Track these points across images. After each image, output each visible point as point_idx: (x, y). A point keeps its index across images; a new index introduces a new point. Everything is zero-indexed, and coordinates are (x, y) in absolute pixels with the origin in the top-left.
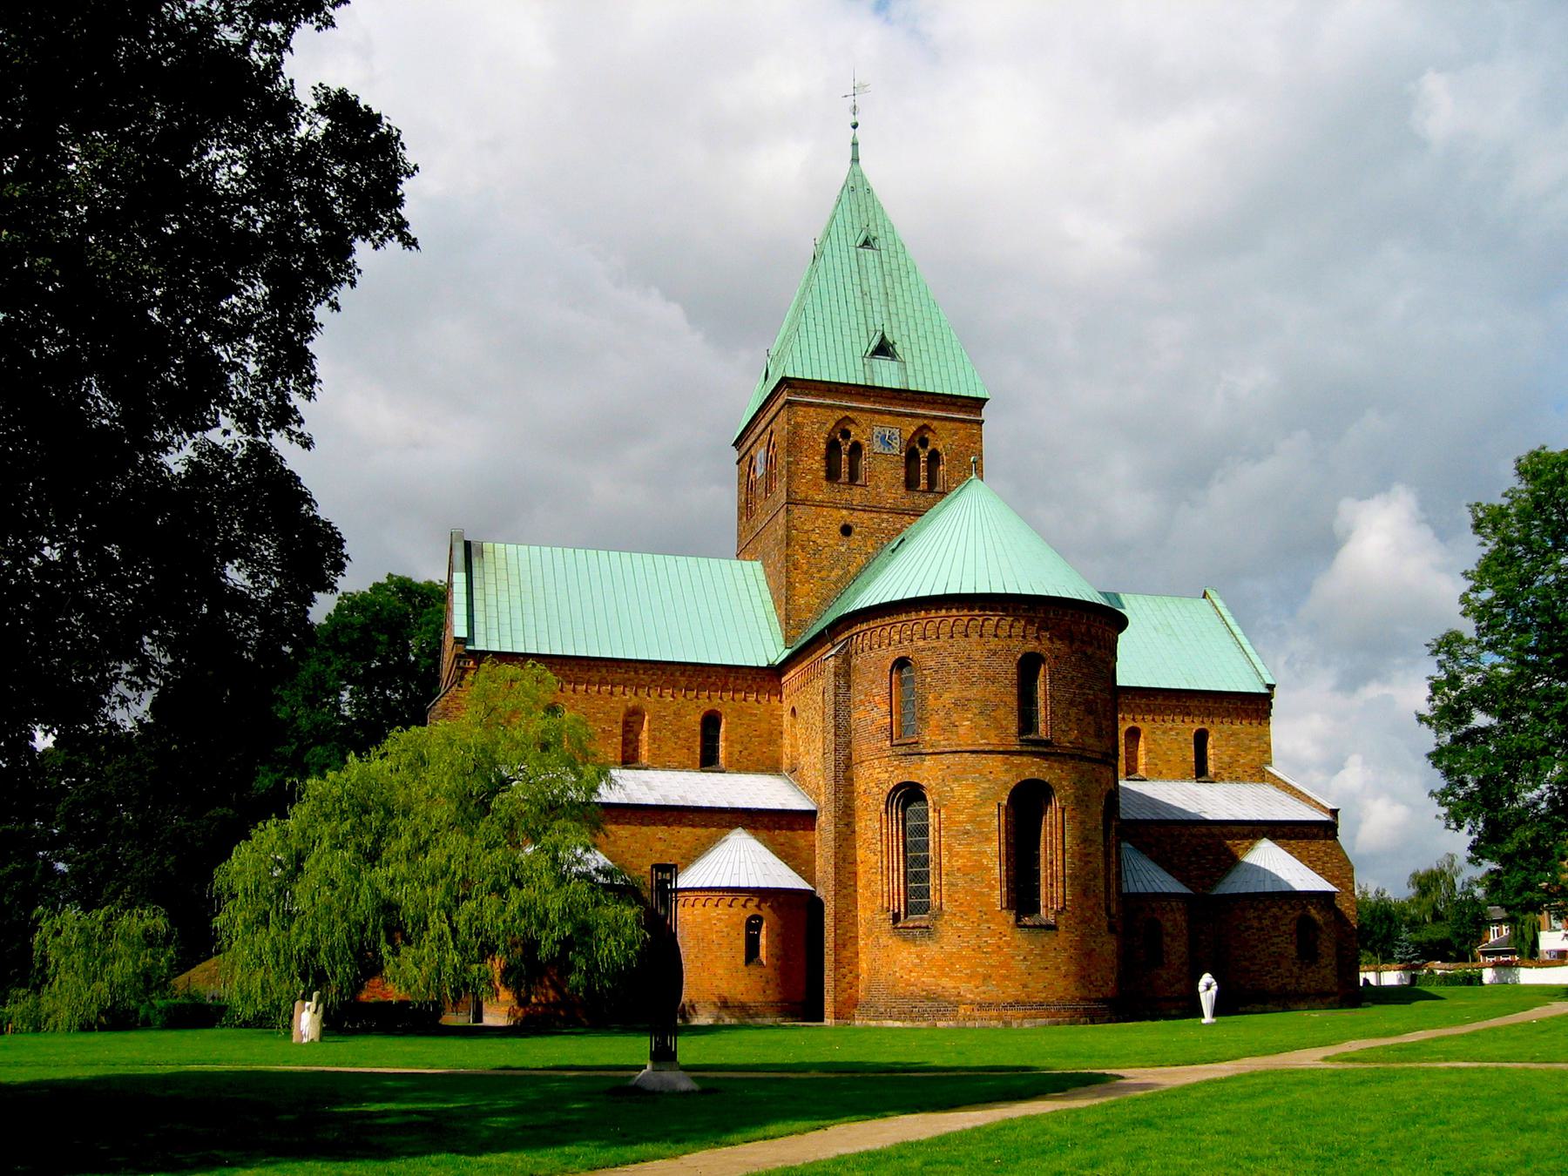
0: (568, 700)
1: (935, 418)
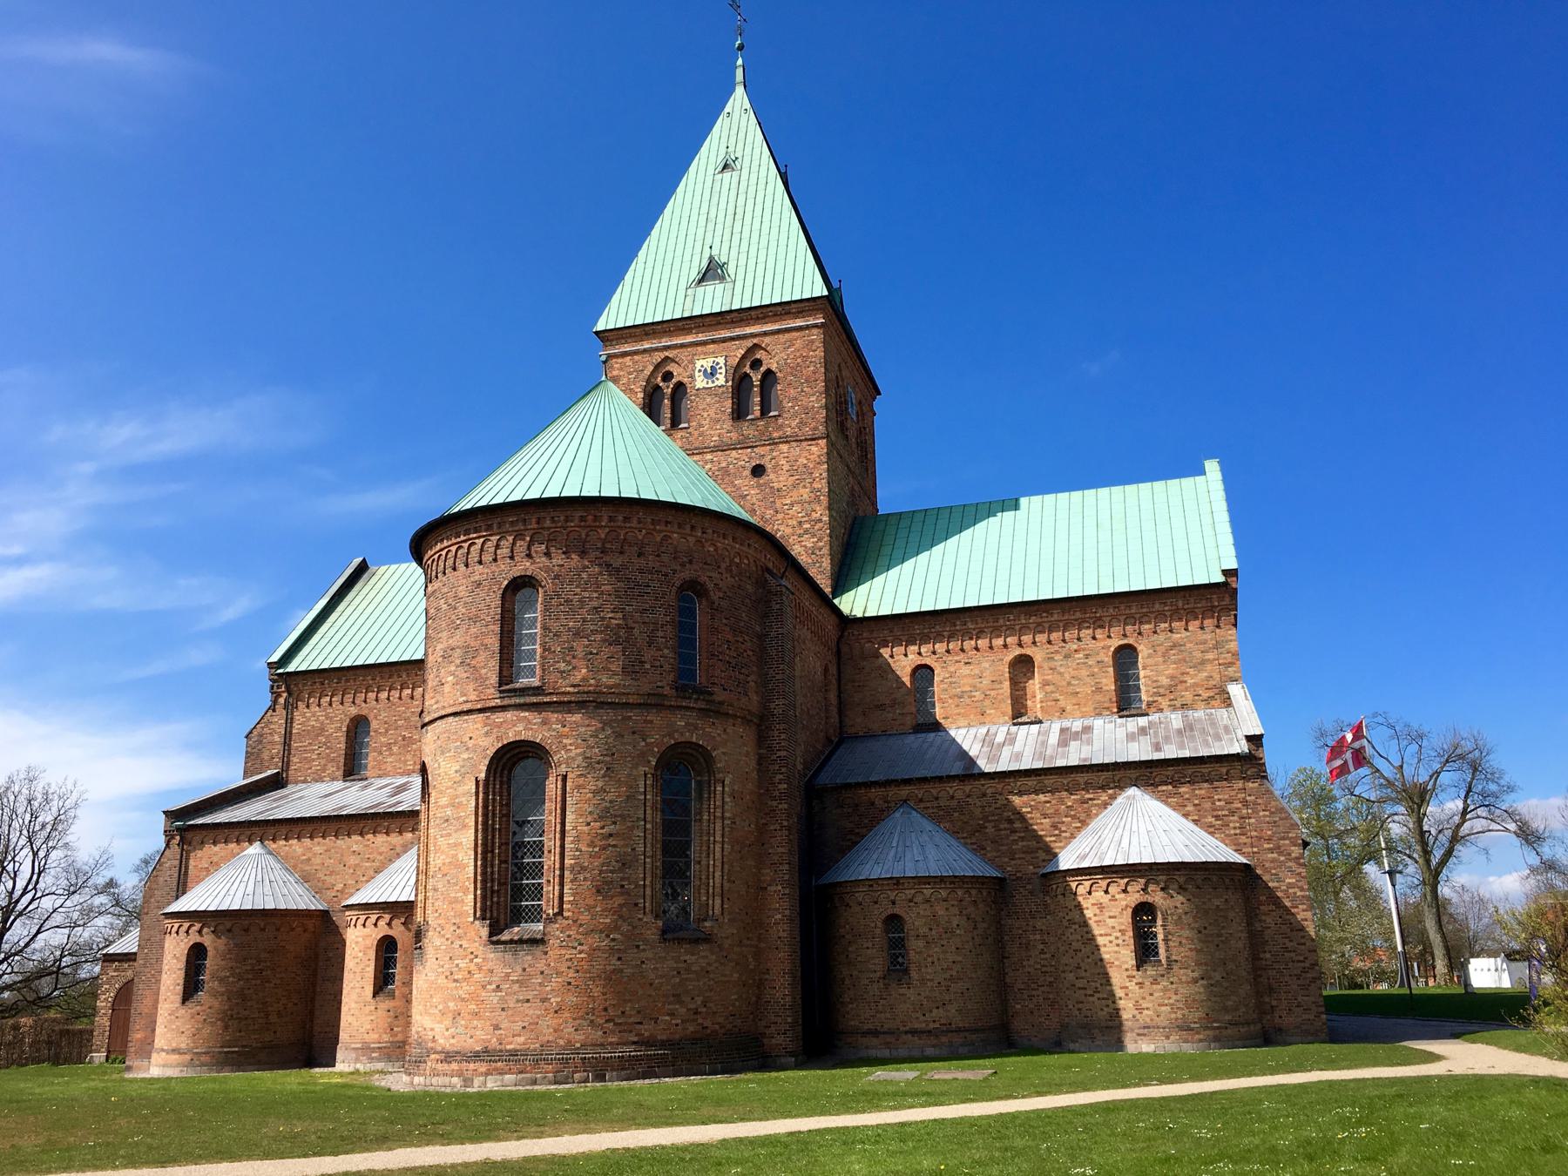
0: (371, 710)
1: (765, 334)
